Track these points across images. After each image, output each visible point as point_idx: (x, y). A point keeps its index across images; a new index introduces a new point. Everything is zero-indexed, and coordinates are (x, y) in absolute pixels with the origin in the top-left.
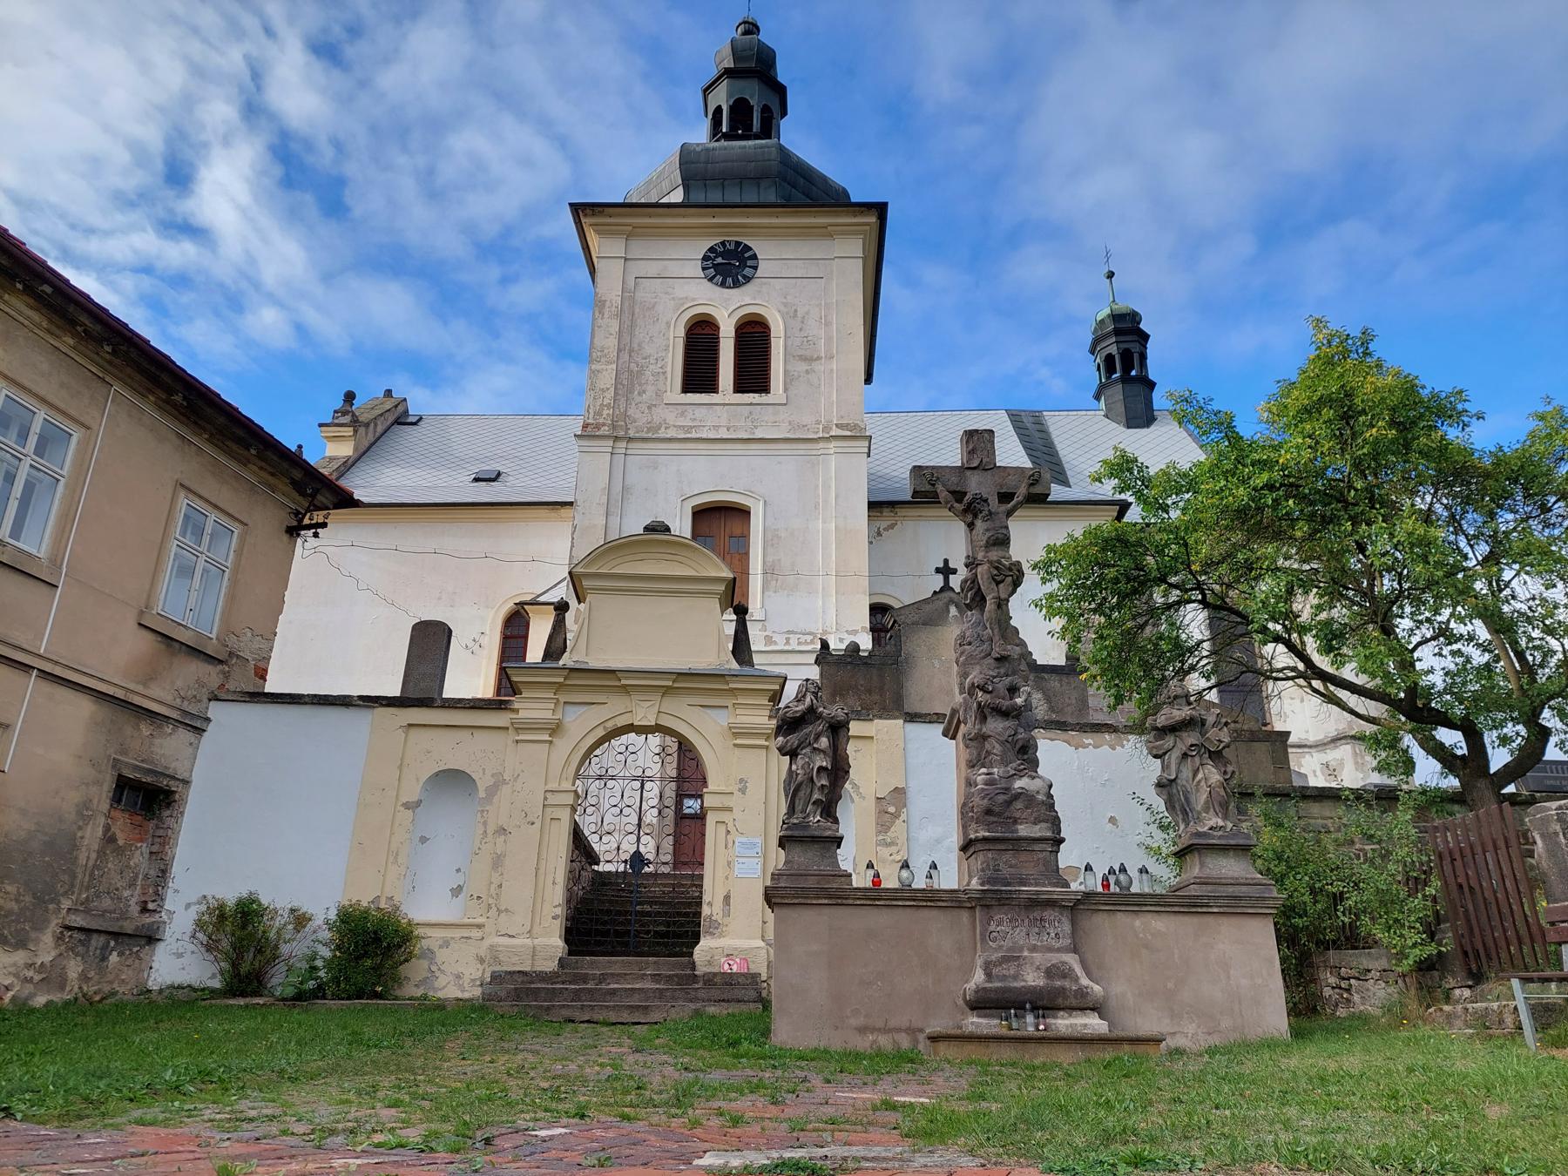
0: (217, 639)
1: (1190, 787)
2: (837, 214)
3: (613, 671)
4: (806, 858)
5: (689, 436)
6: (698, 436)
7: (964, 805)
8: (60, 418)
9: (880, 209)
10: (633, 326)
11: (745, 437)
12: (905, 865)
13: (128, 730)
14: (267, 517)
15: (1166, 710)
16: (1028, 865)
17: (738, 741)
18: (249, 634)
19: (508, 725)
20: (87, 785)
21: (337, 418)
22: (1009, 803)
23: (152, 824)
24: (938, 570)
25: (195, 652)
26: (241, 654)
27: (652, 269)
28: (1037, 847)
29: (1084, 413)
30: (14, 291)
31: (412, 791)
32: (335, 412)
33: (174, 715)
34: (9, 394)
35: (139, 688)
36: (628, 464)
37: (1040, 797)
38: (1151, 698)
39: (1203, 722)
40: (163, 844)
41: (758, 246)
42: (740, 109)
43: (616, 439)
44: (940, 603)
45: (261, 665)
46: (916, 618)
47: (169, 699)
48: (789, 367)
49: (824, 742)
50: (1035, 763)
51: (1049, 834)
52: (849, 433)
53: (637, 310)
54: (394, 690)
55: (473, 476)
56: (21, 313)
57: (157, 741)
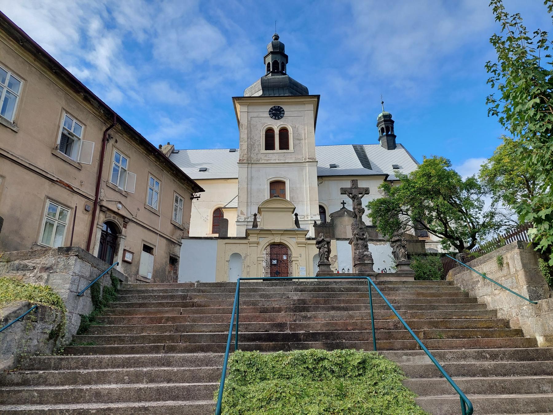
1: (399, 253)
2: (306, 98)
3: (270, 230)
4: (324, 268)
5: (268, 162)
6: (270, 162)
7: (354, 257)
9: (318, 97)
10: (251, 131)
11: (283, 162)
12: (344, 269)
13: (171, 246)
14: (187, 196)
15: (394, 238)
16: (367, 268)
17: (299, 245)
19: (247, 242)
22: (363, 257)
23: (173, 267)
24: (342, 203)
25: (179, 228)
27: (255, 115)
28: (369, 265)
29: (375, 145)
30: (152, 155)
31: (228, 258)
33: (177, 242)
34: (122, 167)
36: (252, 171)
37: (369, 255)
38: (392, 234)
39: (401, 240)
40: (176, 271)
41: (285, 108)
42: (275, 63)
43: (248, 163)
44: (342, 212)
46: (337, 215)
47: (176, 239)
48: (294, 142)
49: (326, 246)
50: (368, 249)
51: (371, 262)
52: (311, 160)
53: (252, 127)
56: (151, 159)
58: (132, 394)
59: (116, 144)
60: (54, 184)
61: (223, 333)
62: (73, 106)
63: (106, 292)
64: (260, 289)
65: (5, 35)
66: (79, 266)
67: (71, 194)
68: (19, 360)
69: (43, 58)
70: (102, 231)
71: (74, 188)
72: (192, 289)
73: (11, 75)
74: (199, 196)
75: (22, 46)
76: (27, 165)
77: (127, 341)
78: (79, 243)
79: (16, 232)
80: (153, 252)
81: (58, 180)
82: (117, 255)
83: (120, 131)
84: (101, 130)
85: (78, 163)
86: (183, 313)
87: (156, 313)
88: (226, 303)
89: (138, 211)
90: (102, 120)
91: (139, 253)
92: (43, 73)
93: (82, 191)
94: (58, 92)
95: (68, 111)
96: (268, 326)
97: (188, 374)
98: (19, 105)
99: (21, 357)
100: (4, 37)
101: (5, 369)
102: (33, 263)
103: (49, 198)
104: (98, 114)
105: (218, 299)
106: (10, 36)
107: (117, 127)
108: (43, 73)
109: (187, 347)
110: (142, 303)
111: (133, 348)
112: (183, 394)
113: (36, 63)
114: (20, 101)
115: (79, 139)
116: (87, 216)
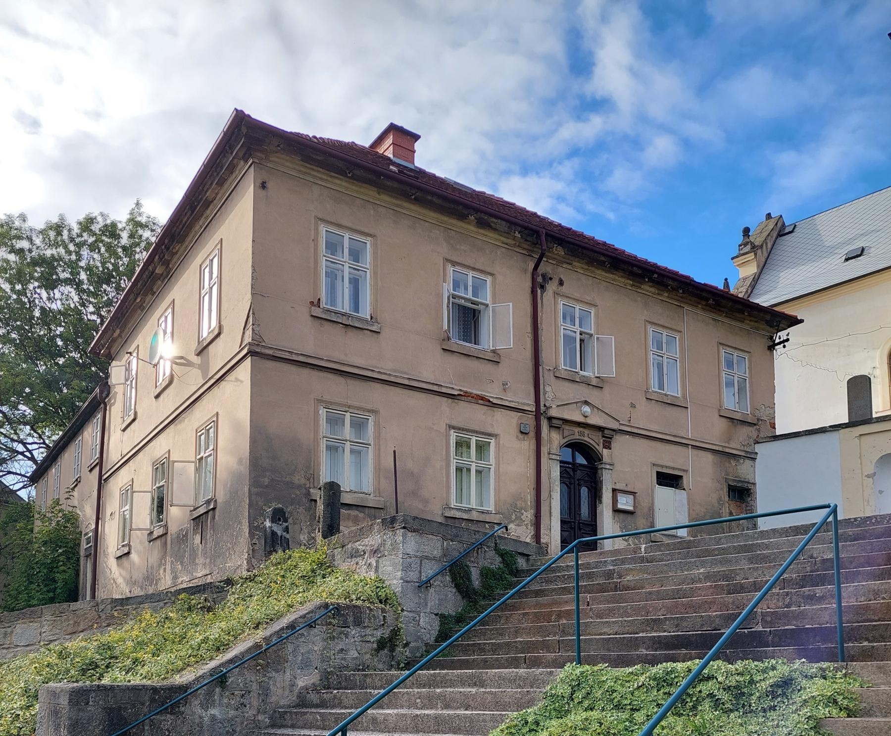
0: (751, 414)
8: (671, 332)
13: (727, 464)
14: (758, 345)
18: (763, 408)
20: (718, 490)
21: (742, 249)
23: (744, 505)
25: (744, 422)
26: (762, 418)
32: (740, 246)
33: (743, 454)
35: (727, 445)
45: (772, 421)
47: (738, 447)
54: (846, 420)
55: (844, 258)
57: (738, 467)
58: (408, 722)
59: (560, 288)
60: (456, 401)
61: (636, 635)
62: (462, 248)
63: (486, 576)
64: (759, 545)
65: (323, 173)
66: (413, 543)
67: (489, 411)
68: (326, 676)
69: (389, 183)
70: (561, 462)
71: (491, 400)
72: (630, 558)
73: (350, 238)
74: (785, 338)
75: (352, 178)
76: (406, 382)
77: (489, 651)
78: (520, 493)
79: (414, 494)
80: (682, 483)
81: (462, 393)
82: (601, 502)
83: (564, 260)
84: (525, 271)
85: (492, 350)
86: (591, 603)
87: (550, 605)
88: (673, 580)
89: (631, 409)
90: (521, 251)
91: (650, 491)
92: (398, 209)
93: (507, 400)
94: (431, 232)
95: (457, 261)
96: (718, 619)
97: (489, 697)
98: (372, 284)
99: (328, 673)
100: (325, 178)
101: (308, 687)
102: (363, 546)
103: (454, 428)
104: (513, 242)
105: (666, 572)
106: (331, 171)
107: (556, 252)
108: (398, 209)
109: (556, 660)
110: (539, 590)
111: (485, 661)
112: (465, 726)
113: (384, 197)
114: (372, 275)
115: (487, 305)
116: (526, 443)
